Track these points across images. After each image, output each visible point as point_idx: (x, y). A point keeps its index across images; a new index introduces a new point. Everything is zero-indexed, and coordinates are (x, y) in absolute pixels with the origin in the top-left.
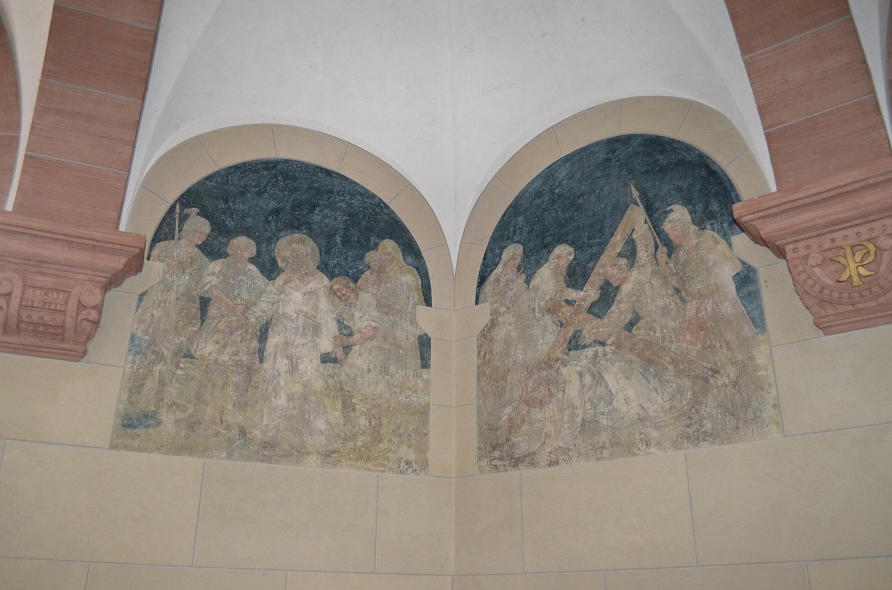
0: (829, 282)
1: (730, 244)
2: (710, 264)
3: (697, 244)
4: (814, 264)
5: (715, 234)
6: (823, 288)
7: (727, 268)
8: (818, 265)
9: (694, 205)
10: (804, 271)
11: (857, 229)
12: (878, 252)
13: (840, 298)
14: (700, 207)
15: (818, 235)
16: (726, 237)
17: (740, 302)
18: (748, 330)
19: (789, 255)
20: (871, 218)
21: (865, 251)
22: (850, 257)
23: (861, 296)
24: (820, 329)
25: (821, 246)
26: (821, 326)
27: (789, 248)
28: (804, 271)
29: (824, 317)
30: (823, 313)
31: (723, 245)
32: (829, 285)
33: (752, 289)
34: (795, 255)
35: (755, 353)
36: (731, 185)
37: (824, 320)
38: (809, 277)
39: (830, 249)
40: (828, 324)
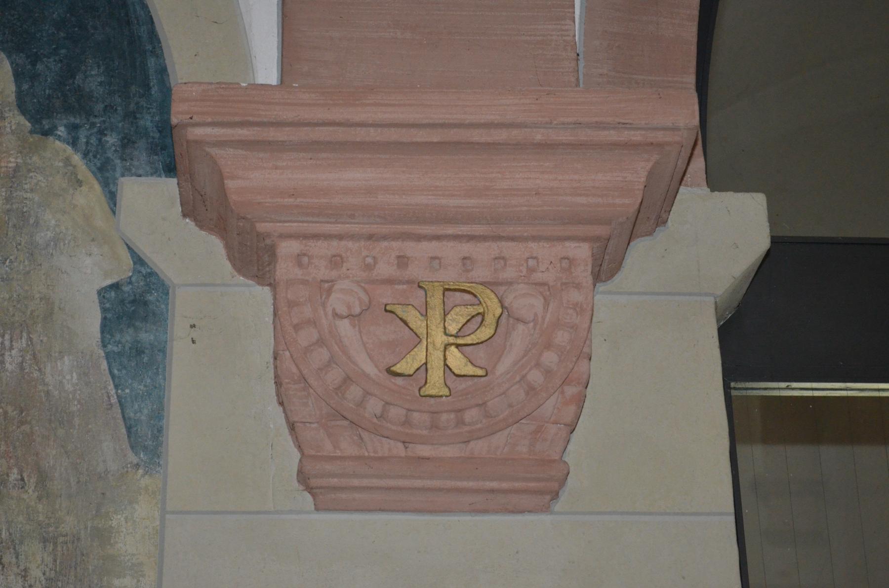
0: (370, 369)
1: (112, 198)
2: (42, 237)
3: (17, 169)
4: (342, 310)
5: (77, 158)
6: (348, 380)
7: (88, 261)
8: (350, 316)
9: (35, 59)
10: (312, 322)
11: (467, 248)
12: (503, 320)
13: (381, 417)
14: (49, 69)
15: (370, 237)
16: (105, 173)
17: (104, 365)
18: (110, 450)
19: (284, 269)
20: (509, 230)
21: (472, 310)
22: (436, 314)
23: (434, 426)
24: (310, 489)
25: (369, 268)
26: (314, 482)
27: (287, 248)
28: (312, 322)
29: (331, 459)
30: (328, 448)
31: (90, 195)
32: (366, 376)
33: (146, 337)
34: (298, 273)
35: (117, 520)
36: (153, 36)
37: (328, 467)
38: (321, 342)
39: (390, 281)
40: (334, 481)
